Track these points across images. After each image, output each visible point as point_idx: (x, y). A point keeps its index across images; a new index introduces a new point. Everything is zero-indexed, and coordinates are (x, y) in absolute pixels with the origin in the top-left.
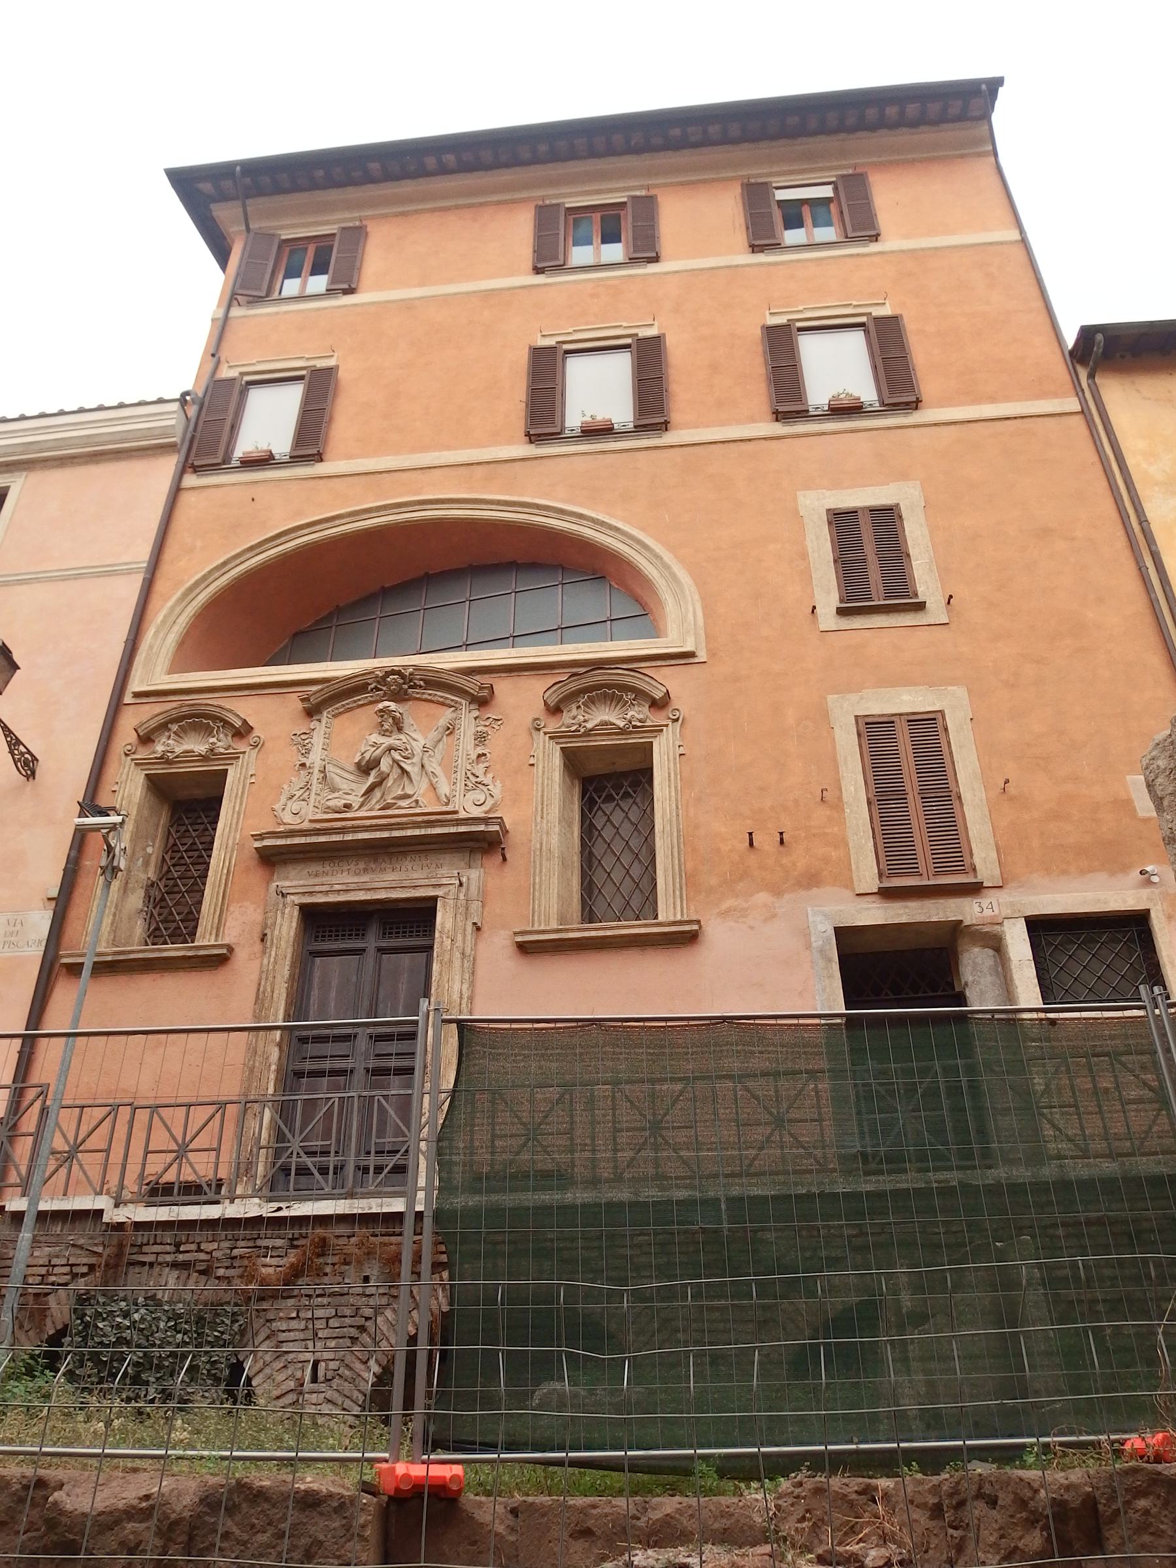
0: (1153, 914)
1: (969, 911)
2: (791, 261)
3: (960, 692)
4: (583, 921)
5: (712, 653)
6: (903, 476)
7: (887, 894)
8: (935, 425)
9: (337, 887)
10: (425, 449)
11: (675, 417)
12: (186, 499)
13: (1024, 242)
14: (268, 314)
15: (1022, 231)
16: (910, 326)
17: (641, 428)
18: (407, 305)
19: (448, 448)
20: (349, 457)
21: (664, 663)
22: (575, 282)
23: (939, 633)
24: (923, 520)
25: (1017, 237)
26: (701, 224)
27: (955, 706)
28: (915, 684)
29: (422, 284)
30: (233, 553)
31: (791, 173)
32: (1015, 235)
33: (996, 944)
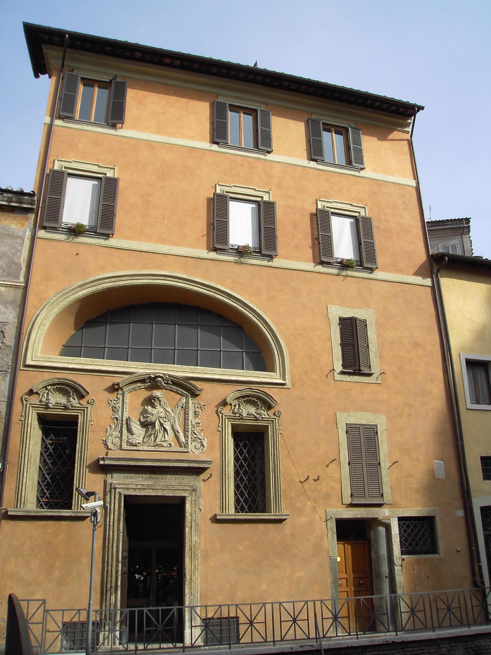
0: (436, 518)
1: (383, 513)
2: (343, 174)
3: (383, 417)
4: (239, 508)
5: (293, 385)
6: (367, 305)
7: (352, 505)
8: (141, 251)
9: (139, 486)
10: (164, 241)
11: (280, 250)
12: (38, 244)
13: (418, 189)
14: (76, 129)
15: (418, 183)
16: (121, 185)
17: (93, 231)
18: (150, 144)
19: (175, 243)
20: (126, 238)
21: (273, 386)
22: (231, 154)
23: (378, 388)
24: (374, 331)
25: (415, 185)
26: (289, 133)
27: (381, 422)
28: (368, 411)
29: (157, 133)
30: (258, 310)
31: (243, 99)
32: (413, 183)
33: (388, 528)
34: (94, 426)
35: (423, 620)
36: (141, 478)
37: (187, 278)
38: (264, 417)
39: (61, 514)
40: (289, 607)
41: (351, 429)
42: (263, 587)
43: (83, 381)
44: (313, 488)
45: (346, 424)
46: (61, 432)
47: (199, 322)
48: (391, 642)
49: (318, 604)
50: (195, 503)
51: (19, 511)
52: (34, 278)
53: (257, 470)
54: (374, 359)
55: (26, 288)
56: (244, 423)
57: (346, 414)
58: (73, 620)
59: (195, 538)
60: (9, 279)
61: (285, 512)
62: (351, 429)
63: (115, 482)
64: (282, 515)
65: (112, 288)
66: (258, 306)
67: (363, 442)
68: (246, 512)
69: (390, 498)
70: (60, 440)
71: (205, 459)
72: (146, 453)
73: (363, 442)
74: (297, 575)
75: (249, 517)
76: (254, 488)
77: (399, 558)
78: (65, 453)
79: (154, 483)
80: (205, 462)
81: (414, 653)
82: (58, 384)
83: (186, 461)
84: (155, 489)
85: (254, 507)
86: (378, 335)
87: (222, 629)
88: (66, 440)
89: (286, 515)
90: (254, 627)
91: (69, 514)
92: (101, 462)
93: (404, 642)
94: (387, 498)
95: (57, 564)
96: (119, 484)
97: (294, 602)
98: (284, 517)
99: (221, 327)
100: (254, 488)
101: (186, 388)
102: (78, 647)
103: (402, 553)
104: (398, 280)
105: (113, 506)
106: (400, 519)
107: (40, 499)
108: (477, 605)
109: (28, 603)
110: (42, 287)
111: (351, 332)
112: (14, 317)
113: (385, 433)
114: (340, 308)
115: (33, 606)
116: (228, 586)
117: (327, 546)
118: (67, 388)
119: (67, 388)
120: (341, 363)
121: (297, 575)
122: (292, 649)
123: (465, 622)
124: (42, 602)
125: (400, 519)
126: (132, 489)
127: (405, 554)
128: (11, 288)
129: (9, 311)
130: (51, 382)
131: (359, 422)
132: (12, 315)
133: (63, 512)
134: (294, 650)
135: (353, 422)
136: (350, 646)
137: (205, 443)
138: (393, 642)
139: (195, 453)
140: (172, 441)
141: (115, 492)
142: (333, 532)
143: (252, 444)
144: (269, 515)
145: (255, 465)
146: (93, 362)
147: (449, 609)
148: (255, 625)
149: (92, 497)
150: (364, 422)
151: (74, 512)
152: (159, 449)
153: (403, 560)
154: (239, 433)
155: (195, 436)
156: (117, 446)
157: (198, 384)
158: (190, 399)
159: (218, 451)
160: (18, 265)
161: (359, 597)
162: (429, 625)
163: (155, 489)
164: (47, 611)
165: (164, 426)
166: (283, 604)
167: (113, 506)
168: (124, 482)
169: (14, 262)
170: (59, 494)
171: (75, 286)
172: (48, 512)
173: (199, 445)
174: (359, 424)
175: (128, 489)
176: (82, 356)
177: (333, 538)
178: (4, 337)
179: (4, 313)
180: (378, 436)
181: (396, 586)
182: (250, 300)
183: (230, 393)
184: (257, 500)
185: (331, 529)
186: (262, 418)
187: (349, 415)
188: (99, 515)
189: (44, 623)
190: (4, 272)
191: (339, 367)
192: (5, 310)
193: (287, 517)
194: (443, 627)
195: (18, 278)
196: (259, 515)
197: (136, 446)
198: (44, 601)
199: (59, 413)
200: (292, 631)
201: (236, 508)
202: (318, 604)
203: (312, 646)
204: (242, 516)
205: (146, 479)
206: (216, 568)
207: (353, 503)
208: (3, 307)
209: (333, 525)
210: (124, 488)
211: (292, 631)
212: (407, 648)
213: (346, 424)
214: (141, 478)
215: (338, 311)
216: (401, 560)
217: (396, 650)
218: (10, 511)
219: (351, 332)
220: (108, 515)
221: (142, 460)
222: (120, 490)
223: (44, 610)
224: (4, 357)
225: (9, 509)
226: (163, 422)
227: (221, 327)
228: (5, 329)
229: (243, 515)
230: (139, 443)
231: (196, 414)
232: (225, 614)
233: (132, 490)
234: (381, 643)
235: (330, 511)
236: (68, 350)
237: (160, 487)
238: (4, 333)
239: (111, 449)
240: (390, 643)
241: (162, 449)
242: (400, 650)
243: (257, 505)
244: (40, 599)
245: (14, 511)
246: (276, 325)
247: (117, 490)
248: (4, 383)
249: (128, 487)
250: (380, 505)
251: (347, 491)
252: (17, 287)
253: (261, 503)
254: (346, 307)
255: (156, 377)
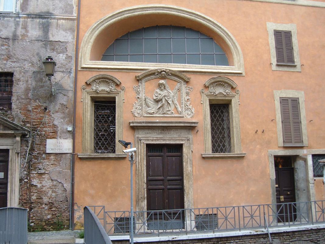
1: (302, 152)
3: (303, 92)
5: (246, 74)
6: (291, 21)
24: (296, 38)
27: (301, 95)
28: (293, 89)
33: (305, 160)
34: (125, 103)
35: (259, 222)
36: (155, 134)
37: (177, 8)
38: (229, 94)
39: (109, 156)
40: (249, 208)
41: (284, 101)
42: (231, 197)
43: (118, 76)
44: (258, 137)
45: (280, 98)
46: (105, 107)
47: (171, 36)
48: (310, 229)
49: (241, 209)
50: (189, 147)
51: (84, 155)
52: (83, 14)
53: (225, 127)
54: (297, 56)
55: (78, 19)
56: (216, 98)
57: (279, 91)
58: (122, 217)
59: (190, 169)
60: (66, 15)
61: (243, 152)
62: (284, 101)
63: (140, 136)
64: (207, 154)
65: (130, 17)
66: (222, 25)
67: (290, 107)
68: (219, 152)
69: (307, 143)
70: (105, 112)
71: (194, 121)
72: (158, 119)
73: (290, 107)
74: (251, 189)
75: (222, 156)
76: (221, 138)
77: (313, 179)
78: (109, 120)
79: (164, 136)
80: (194, 123)
81: (239, 243)
82: (102, 78)
83: (182, 122)
84: (164, 140)
85: (224, 149)
86: (299, 41)
87: (206, 221)
88: (109, 112)
89: (244, 154)
90: (228, 220)
91: (114, 156)
92: (131, 125)
93: (318, 229)
94: (305, 143)
95: (109, 186)
96: (143, 137)
97: (251, 206)
98: (243, 155)
99: (200, 39)
100: (221, 138)
101: (182, 78)
102: (125, 231)
103: (314, 176)
104: (311, 4)
105: (140, 151)
106: (314, 156)
107: (96, 147)
108: (271, 215)
109: (95, 208)
110: (87, 18)
111: (283, 40)
112: (72, 38)
113: (304, 103)
114: (274, 24)
115: (98, 210)
116: (210, 196)
117: (269, 172)
118: (105, 80)
119: (105, 80)
120: (275, 59)
121: (251, 189)
122: (251, 233)
123: (237, 227)
124: (103, 207)
125: (314, 156)
126: (151, 140)
127: (316, 177)
128: (68, 21)
129: (69, 35)
130: (97, 77)
131: (288, 96)
132: (70, 37)
133: (111, 155)
134: (252, 234)
135: (284, 96)
136: (285, 231)
137: (193, 111)
138: (311, 229)
139: (188, 117)
140: (173, 110)
141: (141, 142)
142: (272, 164)
143: (220, 110)
144: (234, 154)
145: (224, 124)
146: (122, 63)
147: (252, 216)
148: (224, 218)
149: (129, 146)
150: (291, 96)
151: (117, 155)
152: (166, 116)
153: (315, 180)
154: (213, 105)
155: (187, 107)
156: (140, 115)
157: (188, 75)
158: (183, 85)
159: (202, 117)
160: (71, 6)
161: (291, 203)
162: (237, 227)
163: (164, 140)
164: (106, 212)
165: (168, 101)
166: (219, 208)
167: (140, 151)
168: (145, 136)
169: (69, 4)
170: (107, 144)
171: (108, 17)
172: (101, 155)
173: (190, 113)
174: (288, 98)
175: (148, 140)
176: (129, 60)
177: (272, 168)
178: (67, 51)
179: (66, 36)
180: (299, 105)
181: (310, 196)
182: (217, 21)
183: (206, 80)
184: (226, 145)
185: (271, 162)
186: (228, 95)
187: (281, 92)
188: (134, 156)
189: (104, 219)
190: (63, 10)
191: (274, 61)
192: (66, 34)
193: (245, 155)
194: (272, 226)
195: (72, 14)
196: (227, 154)
197: (152, 114)
198: (104, 207)
199: (103, 96)
200: (251, 222)
201: (213, 150)
202: (241, 209)
203: (262, 231)
204: (217, 155)
205: (158, 134)
206: (203, 186)
207: (285, 146)
208: (65, 32)
209: (272, 160)
210: (146, 140)
211: (251, 222)
212: (319, 232)
213: (280, 98)
214: (155, 134)
215: (272, 26)
216: (314, 180)
217: (312, 233)
218: (80, 155)
219: (283, 40)
220: (138, 156)
221: (172, 123)
222: (143, 141)
223: (104, 212)
224: (68, 64)
225: (78, 154)
226: (167, 99)
227: (200, 39)
228: (67, 46)
229: (218, 154)
230: (153, 113)
231: (187, 94)
232: (210, 212)
233: (150, 141)
234: (304, 229)
235: (270, 151)
236: (105, 57)
237: (167, 138)
238: (66, 49)
239: (136, 117)
240: (309, 230)
241: (167, 116)
242: (315, 234)
243: (225, 148)
244: (101, 205)
245: (82, 155)
246: (235, 36)
247: (142, 141)
248: (69, 79)
249: (148, 139)
250: (302, 147)
251: (281, 140)
252: (73, 20)
253: (228, 147)
254: (278, 23)
255: (162, 71)
